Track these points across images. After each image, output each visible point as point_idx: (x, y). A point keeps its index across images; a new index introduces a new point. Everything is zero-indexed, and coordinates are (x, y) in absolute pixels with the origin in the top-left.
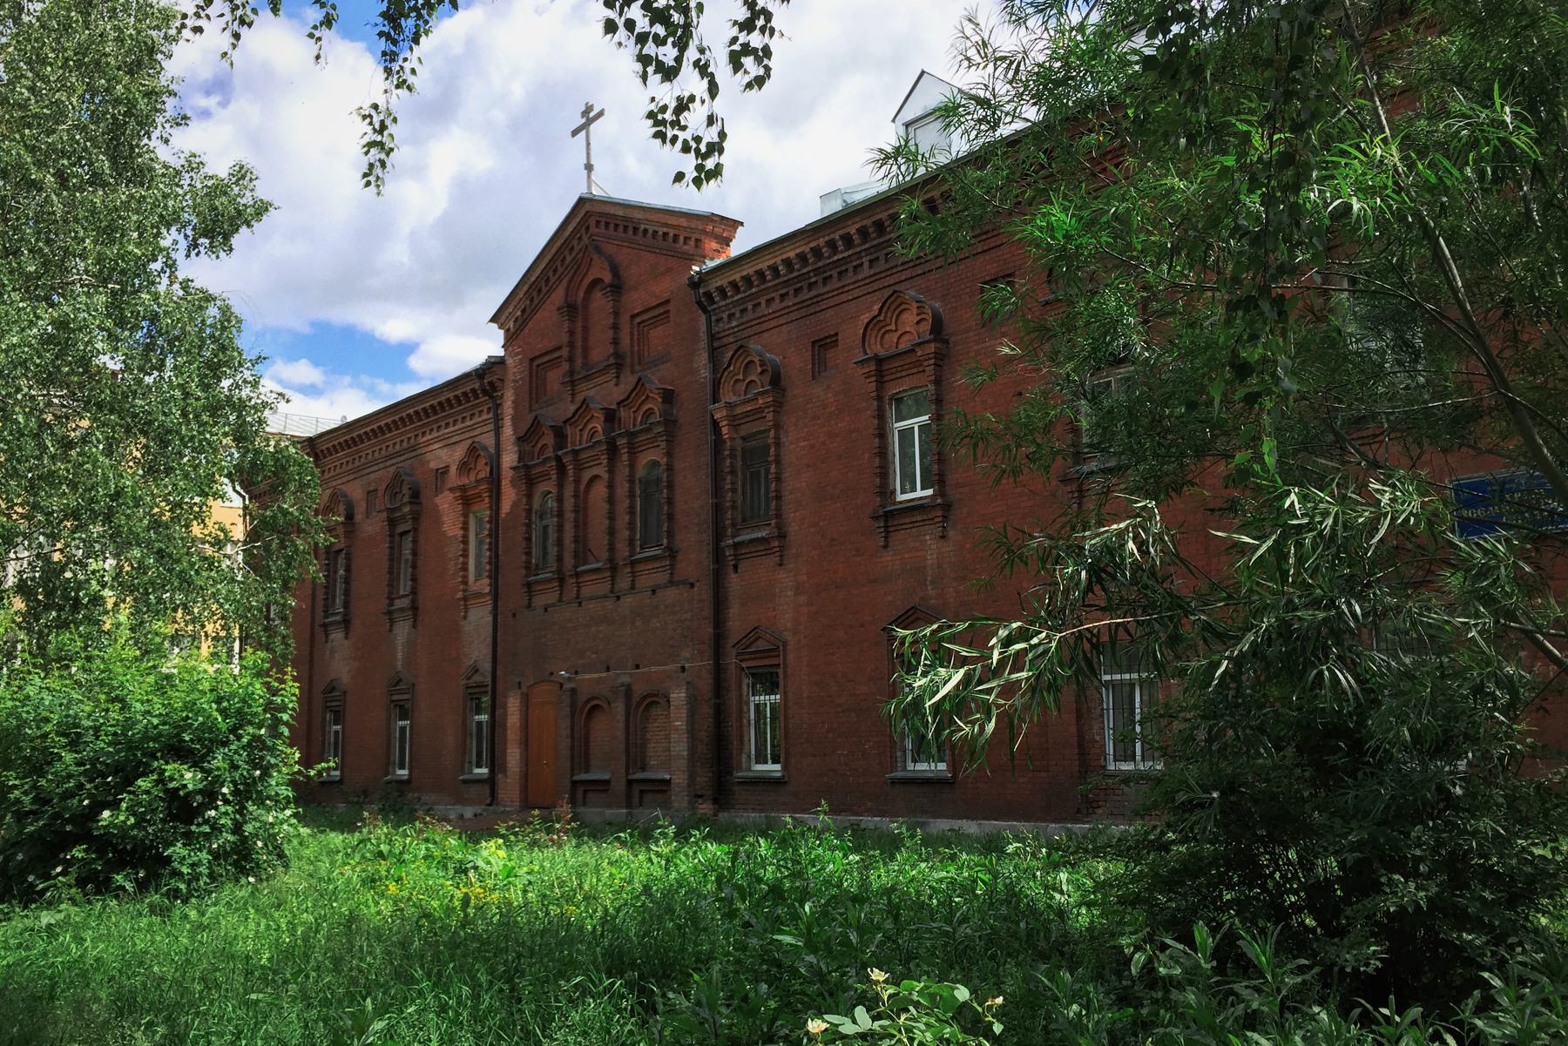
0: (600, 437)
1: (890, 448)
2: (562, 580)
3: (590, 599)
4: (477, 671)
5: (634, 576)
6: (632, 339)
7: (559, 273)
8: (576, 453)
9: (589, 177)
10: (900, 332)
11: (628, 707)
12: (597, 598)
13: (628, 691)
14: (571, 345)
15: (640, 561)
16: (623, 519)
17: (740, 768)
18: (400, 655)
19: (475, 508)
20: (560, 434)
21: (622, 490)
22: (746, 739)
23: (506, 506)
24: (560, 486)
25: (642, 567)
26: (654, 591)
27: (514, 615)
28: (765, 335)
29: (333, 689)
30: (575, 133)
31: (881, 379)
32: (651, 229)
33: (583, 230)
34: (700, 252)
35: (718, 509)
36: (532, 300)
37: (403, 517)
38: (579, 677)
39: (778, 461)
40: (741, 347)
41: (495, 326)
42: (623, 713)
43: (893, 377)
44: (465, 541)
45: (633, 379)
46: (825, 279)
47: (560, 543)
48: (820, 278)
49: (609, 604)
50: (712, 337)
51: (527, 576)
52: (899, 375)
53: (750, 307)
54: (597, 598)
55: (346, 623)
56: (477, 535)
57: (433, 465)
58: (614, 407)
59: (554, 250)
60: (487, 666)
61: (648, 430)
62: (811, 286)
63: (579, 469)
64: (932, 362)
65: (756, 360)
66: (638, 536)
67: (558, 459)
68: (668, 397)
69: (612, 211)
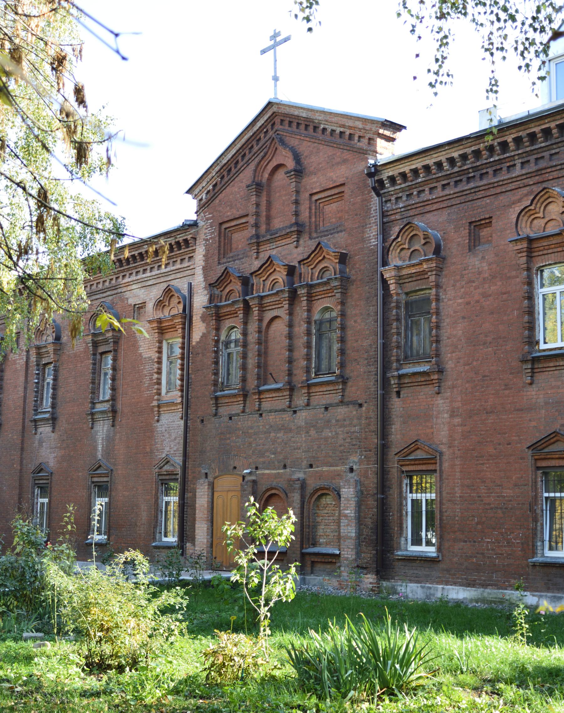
0: (280, 286)
1: (536, 308)
2: (245, 396)
3: (270, 411)
4: (168, 462)
5: (309, 396)
6: (310, 212)
7: (246, 159)
8: (262, 298)
9: (276, 86)
10: (412, 250)
11: (303, 497)
12: (276, 411)
13: (303, 485)
14: (257, 214)
15: (316, 385)
16: (300, 352)
17: (399, 549)
18: (100, 448)
19: (167, 336)
20: (246, 282)
21: (301, 328)
22: (405, 526)
23: (196, 336)
24: (245, 323)
25: (317, 389)
26: (326, 409)
27: (202, 421)
28: (428, 215)
29: (41, 470)
30: (263, 52)
31: (530, 253)
32: (329, 128)
33: (269, 126)
34: (372, 148)
35: (385, 347)
36: (222, 178)
37: (106, 341)
38: (258, 472)
39: (438, 313)
40: (409, 223)
41: (189, 196)
42: (298, 501)
43: (541, 253)
44: (160, 362)
45: (312, 244)
46: (482, 175)
47: (244, 367)
48: (478, 174)
49: (287, 416)
50: (384, 214)
51: (215, 391)
52: (545, 252)
53: (415, 193)
54: (276, 411)
55: (54, 419)
56: (168, 357)
57: (131, 301)
58: (295, 263)
59: (243, 140)
60: (178, 460)
61: (325, 283)
62: (469, 179)
63: (262, 309)
64: (434, 273)
65: (421, 234)
66: (313, 365)
67: (246, 302)
68: (343, 259)
69: (296, 113)
